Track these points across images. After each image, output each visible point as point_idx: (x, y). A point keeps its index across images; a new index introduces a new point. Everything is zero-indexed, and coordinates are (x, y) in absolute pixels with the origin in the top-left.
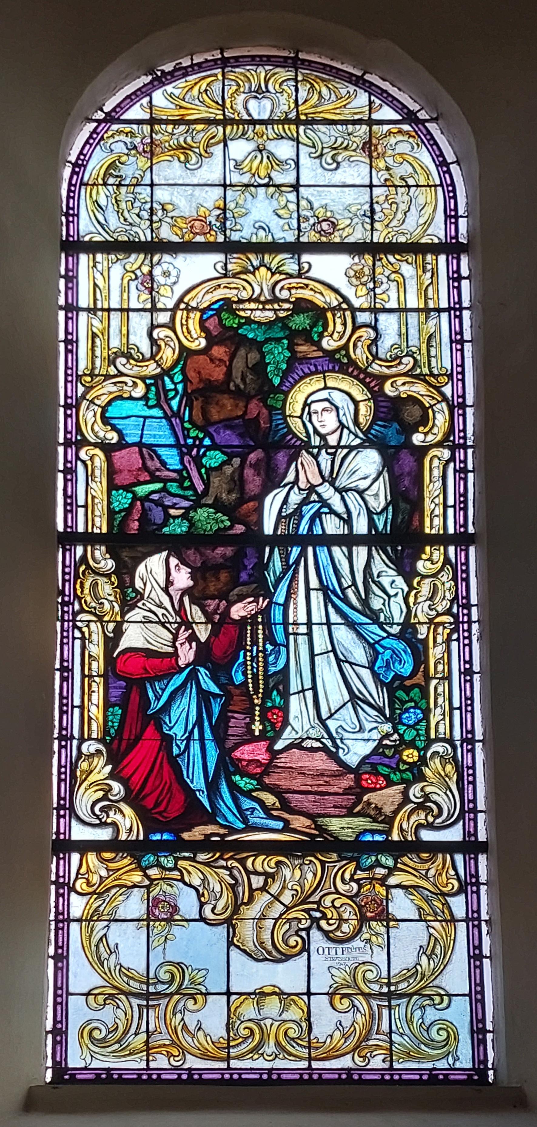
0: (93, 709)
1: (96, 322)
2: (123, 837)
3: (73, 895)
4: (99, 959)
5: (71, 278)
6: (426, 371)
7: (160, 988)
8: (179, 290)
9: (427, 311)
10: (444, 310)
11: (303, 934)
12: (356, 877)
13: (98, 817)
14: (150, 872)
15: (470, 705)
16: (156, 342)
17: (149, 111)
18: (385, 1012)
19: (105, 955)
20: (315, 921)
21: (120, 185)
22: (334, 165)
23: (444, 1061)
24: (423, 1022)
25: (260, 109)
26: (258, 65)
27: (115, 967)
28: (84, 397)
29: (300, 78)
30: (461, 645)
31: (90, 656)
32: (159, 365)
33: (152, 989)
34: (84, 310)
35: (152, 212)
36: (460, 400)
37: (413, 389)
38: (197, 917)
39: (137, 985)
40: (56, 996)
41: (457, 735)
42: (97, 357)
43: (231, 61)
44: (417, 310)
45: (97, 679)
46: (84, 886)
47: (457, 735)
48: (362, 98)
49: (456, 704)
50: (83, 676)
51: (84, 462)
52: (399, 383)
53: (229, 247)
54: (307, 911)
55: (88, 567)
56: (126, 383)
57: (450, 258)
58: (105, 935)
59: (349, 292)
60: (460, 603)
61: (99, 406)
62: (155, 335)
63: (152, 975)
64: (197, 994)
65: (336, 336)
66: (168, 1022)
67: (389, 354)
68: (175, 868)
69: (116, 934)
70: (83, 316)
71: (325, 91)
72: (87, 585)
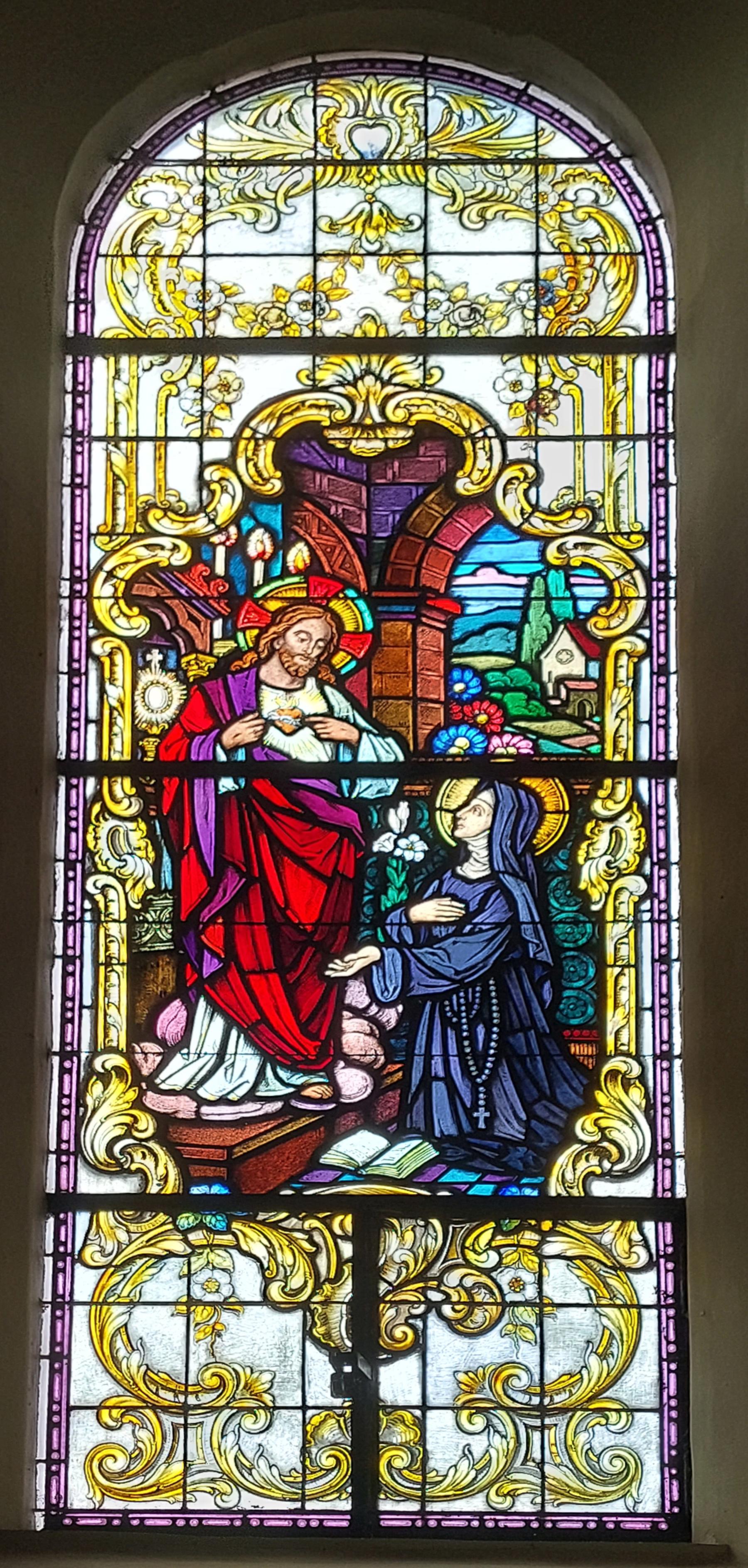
0: (112, 1010)
1: (119, 459)
2: (153, 1189)
3: (79, 1268)
4: (115, 1359)
5: (81, 392)
6: (611, 529)
7: (205, 1398)
8: (241, 411)
9: (614, 438)
10: (640, 437)
11: (419, 1323)
12: (494, 1244)
13: (117, 1160)
14: (191, 1237)
16: (208, 487)
17: (201, 145)
18: (536, 1436)
19: (122, 1353)
20: (432, 1306)
21: (157, 255)
22: (482, 224)
23: (621, 1502)
24: (590, 1449)
25: (371, 141)
26: (368, 75)
27: (139, 1367)
28: (100, 567)
29: (431, 93)
31: (107, 936)
32: (212, 521)
33: (192, 1400)
34: (99, 439)
35: (204, 296)
37: (588, 553)
38: (259, 1298)
39: (170, 1396)
41: (647, 1049)
42: (119, 493)
43: (326, 68)
44: (602, 438)
45: (118, 968)
46: (97, 1256)
47: (647, 1049)
48: (524, 122)
50: (96, 964)
51: (97, 658)
52: (570, 545)
53: (318, 346)
54: (423, 1291)
55: (104, 808)
56: (162, 548)
57: (654, 358)
58: (126, 1325)
60: (655, 860)
61: (122, 580)
62: (207, 475)
63: (192, 1379)
64: (259, 1408)
65: (476, 476)
66: (215, 1445)
67: (555, 503)
68: (228, 1230)
69: (143, 1321)
70: (98, 448)
71: (468, 113)
72: (103, 832)
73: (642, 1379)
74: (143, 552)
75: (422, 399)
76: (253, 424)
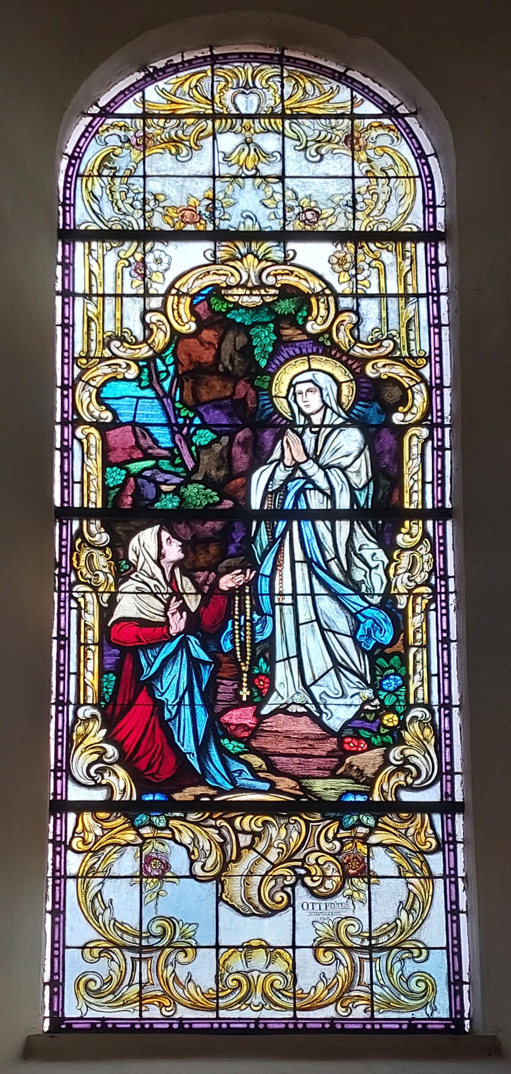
0: (89, 675)
1: (91, 307)
2: (117, 797)
3: (69, 853)
4: (94, 913)
5: (68, 265)
6: (405, 353)
7: (153, 941)
8: (170, 277)
9: (406, 296)
10: (422, 295)
12: (339, 836)
13: (93, 778)
14: (143, 831)
15: (447, 672)
16: (149, 326)
17: (142, 105)
18: (367, 965)
19: (100, 910)
20: (300, 877)
21: (114, 176)
22: (318, 158)
23: (423, 1011)
24: (402, 974)
26: (246, 62)
27: (110, 921)
28: (80, 378)
29: (285, 74)
31: (86, 625)
32: (151, 348)
33: (144, 943)
34: (79, 295)
35: (145, 202)
37: (393, 370)
38: (188, 874)
39: (130, 939)
41: (435, 700)
42: (92, 340)
43: (220, 58)
44: (397, 296)
45: (92, 647)
46: (80, 844)
47: (435, 700)
48: (345, 94)
50: (79, 644)
51: (80, 440)
52: (380, 365)
53: (218, 236)
54: (292, 868)
55: (84, 540)
56: (120, 365)
57: (428, 246)
58: (100, 891)
59: (332, 278)
60: (438, 575)
61: (94, 387)
62: (147, 320)
63: (144, 929)
64: (187, 947)
65: (319, 320)
66: (160, 974)
67: (370, 337)
68: (167, 827)
69: (111, 890)
70: (79, 302)
71: (309, 87)
72: (83, 557)
73: (434, 931)
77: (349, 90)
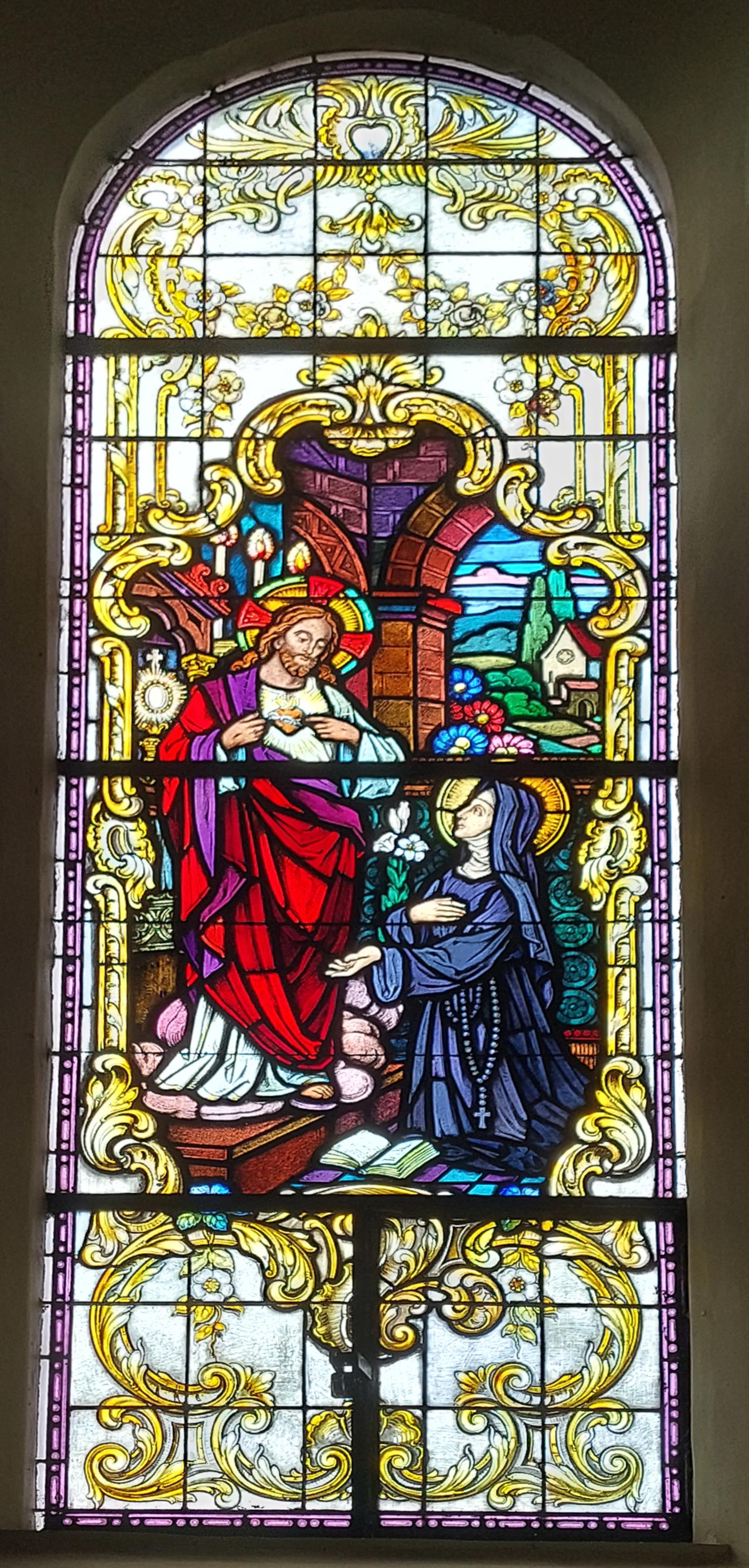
0: (112, 1010)
1: (119, 459)
2: (154, 1189)
3: (79, 1268)
4: (115, 1359)
5: (82, 392)
6: (612, 529)
7: (206, 1398)
8: (241, 411)
9: (615, 438)
10: (641, 437)
12: (494, 1244)
13: (117, 1160)
14: (192, 1237)
15: (666, 911)
16: (209, 487)
17: (201, 145)
18: (537, 1436)
19: (122, 1353)
20: (432, 1306)
21: (157, 255)
22: (482, 224)
23: (622, 1502)
24: (591, 1449)
26: (368, 75)
27: (139, 1367)
28: (100, 567)
29: (431, 93)
30: (658, 1016)
31: (107, 936)
32: (212, 521)
33: (192, 1400)
34: (99, 439)
35: (204, 296)
36: (664, 951)
38: (259, 1298)
39: (170, 1396)
40: (64, 1009)
41: (648, 1049)
42: (119, 493)
43: (327, 68)
44: (603, 438)
45: (118, 968)
46: (97, 1256)
47: (648, 1049)
48: (525, 122)
49: (645, 715)
50: (96, 964)
51: (97, 658)
52: (570, 545)
53: (319, 346)
54: (424, 1291)
55: (105, 808)
56: (163, 548)
57: (655, 358)
58: (126, 1325)
59: (500, 414)
60: (656, 860)
61: (122, 580)
62: (207, 475)
63: (192, 1379)
64: (260, 1408)
65: (477, 476)
66: (216, 1445)
67: (556, 503)
68: (229, 1230)
69: (143, 1321)
70: (98, 448)
71: (469, 113)
72: (103, 832)
74: (144, 552)
75: (423, 399)
76: (253, 424)
77: (534, 118)
